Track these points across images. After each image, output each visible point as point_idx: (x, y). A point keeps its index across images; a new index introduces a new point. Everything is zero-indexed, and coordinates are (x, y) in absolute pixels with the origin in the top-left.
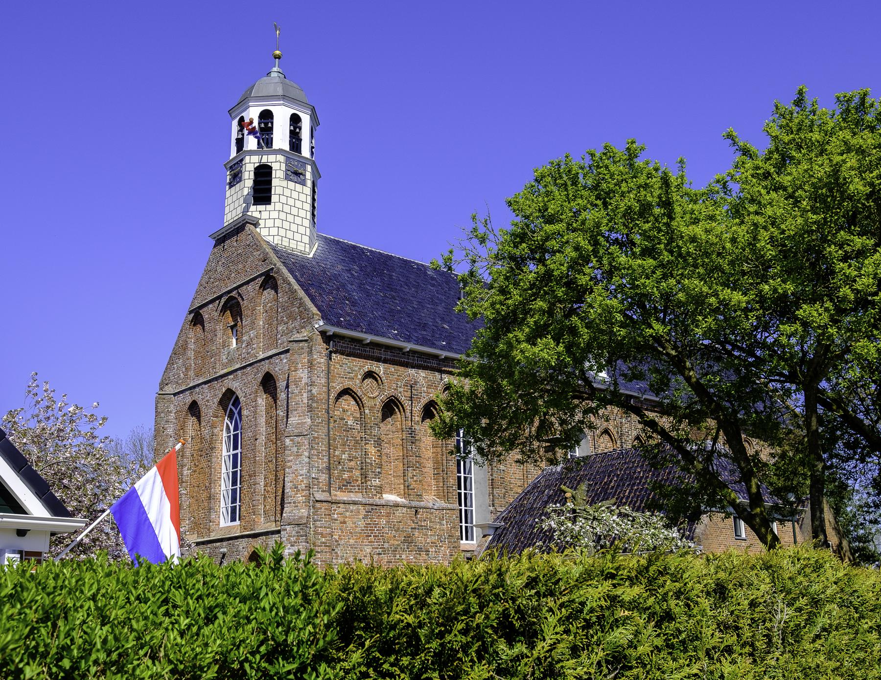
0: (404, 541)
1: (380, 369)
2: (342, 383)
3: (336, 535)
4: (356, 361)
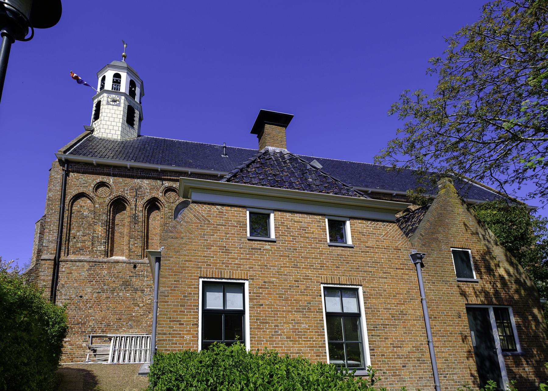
0: (123, 285)
1: (111, 180)
2: (77, 190)
3: (62, 281)
4: (89, 176)
